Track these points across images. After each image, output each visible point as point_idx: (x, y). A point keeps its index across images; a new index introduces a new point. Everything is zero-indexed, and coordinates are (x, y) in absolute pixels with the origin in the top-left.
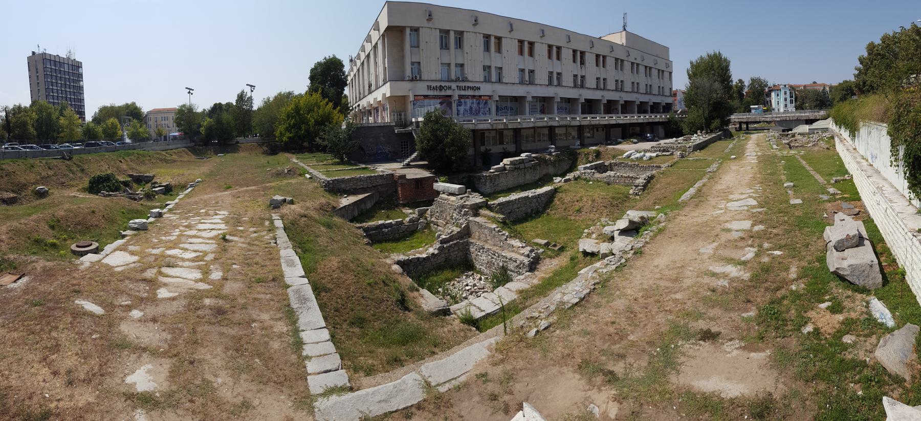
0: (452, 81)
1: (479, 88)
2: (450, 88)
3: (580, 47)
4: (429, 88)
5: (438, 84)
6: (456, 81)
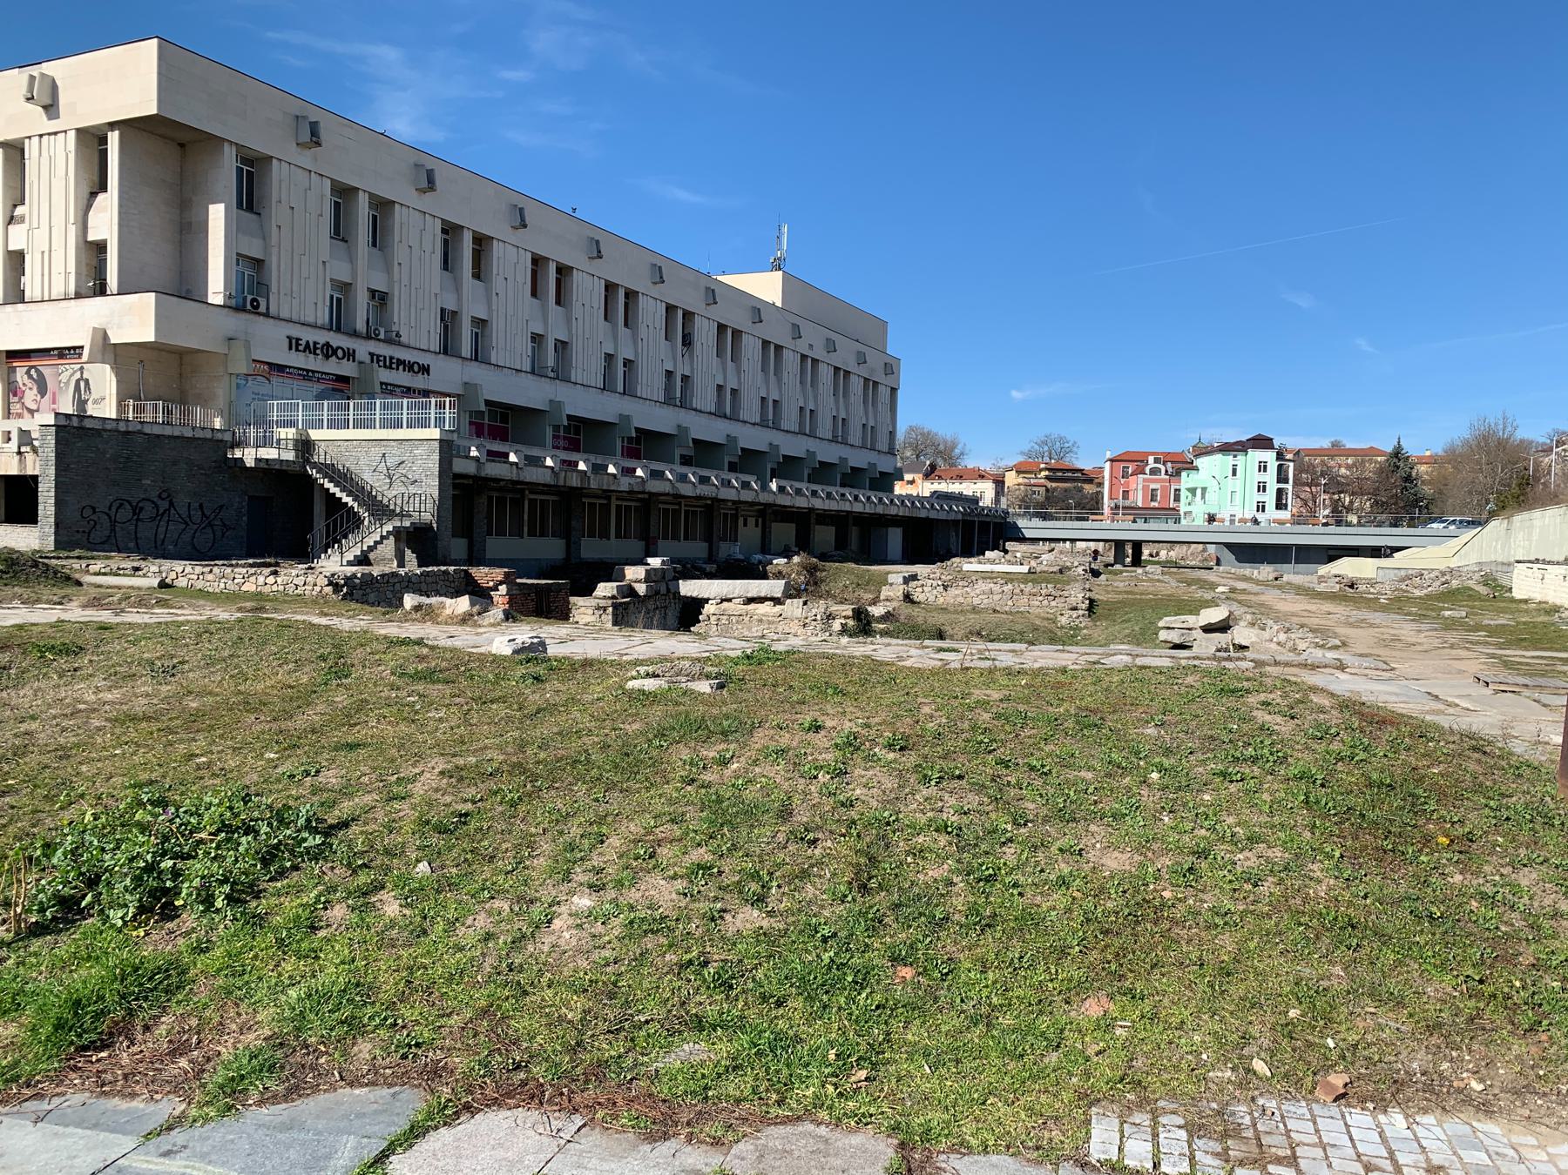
0: (355, 334)
1: (425, 370)
2: (350, 355)
4: (294, 344)
5: (322, 337)
6: (368, 337)
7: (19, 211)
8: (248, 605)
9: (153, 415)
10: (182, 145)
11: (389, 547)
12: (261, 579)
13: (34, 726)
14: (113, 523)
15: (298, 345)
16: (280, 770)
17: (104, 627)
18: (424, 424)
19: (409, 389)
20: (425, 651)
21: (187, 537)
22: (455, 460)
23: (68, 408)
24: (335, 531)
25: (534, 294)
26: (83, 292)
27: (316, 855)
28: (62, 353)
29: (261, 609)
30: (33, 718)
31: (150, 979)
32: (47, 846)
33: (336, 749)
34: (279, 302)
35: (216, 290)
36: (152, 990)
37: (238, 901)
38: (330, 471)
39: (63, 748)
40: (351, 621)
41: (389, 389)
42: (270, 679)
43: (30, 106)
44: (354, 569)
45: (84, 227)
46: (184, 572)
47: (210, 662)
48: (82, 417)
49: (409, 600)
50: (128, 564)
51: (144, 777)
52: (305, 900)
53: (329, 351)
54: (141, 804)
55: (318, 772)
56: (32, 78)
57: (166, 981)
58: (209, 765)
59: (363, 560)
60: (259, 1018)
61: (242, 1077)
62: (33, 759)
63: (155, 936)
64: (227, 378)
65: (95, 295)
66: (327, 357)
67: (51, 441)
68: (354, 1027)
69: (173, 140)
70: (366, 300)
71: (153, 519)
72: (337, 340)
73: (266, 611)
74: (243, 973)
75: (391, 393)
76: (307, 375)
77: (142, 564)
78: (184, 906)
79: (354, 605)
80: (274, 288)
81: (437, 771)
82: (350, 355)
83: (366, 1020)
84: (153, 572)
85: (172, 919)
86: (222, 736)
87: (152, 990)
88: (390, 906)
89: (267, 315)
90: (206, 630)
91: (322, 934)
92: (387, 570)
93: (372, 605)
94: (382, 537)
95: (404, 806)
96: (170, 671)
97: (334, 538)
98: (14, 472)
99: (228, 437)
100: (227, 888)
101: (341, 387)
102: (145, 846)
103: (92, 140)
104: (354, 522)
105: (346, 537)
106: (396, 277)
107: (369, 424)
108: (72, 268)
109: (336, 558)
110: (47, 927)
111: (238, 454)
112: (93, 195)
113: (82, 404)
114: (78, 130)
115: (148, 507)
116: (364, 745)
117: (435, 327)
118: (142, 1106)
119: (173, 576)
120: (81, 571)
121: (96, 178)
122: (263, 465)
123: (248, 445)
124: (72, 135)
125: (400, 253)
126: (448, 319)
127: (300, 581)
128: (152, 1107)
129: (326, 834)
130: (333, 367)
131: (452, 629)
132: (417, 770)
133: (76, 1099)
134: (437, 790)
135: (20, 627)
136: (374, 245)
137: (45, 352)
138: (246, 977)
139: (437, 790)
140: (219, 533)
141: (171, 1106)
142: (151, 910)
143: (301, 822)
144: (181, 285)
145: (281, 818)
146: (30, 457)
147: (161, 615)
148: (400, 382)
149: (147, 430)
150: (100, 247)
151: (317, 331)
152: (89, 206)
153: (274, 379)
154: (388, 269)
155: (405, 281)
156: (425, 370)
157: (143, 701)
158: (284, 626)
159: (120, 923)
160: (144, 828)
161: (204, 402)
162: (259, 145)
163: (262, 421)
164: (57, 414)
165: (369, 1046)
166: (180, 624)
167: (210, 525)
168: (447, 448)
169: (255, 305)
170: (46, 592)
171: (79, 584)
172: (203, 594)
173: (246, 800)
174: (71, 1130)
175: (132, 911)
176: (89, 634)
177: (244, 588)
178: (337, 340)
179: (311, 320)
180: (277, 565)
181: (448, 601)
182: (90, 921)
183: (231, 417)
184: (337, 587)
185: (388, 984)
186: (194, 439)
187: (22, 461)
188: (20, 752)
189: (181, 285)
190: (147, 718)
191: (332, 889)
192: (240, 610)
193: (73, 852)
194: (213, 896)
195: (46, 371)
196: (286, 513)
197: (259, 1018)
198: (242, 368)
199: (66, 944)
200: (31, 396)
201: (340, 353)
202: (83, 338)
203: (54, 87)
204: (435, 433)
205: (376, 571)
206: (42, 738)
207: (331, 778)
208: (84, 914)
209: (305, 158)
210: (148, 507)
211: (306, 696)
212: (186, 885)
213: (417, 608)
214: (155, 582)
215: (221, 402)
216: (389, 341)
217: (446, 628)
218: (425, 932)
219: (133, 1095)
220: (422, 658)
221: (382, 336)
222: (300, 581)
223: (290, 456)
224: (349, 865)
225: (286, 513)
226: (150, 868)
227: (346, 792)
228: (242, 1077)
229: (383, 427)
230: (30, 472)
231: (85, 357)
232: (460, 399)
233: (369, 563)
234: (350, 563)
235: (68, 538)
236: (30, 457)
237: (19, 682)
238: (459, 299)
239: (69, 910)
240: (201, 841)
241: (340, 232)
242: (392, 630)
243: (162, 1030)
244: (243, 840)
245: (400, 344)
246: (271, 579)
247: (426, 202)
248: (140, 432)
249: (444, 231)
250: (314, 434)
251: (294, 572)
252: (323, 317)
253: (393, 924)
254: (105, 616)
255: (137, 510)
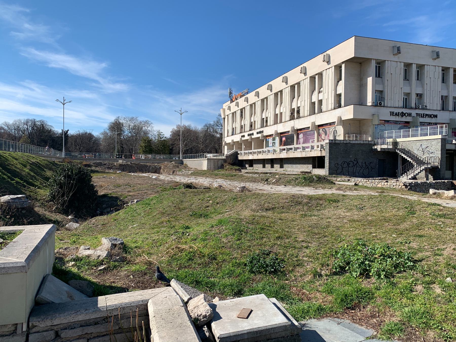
0: (411, 108)
1: (436, 116)
2: (410, 115)
3: (415, 59)
4: (392, 114)
5: (400, 111)
6: (416, 108)
7: (321, 89)
8: (379, 191)
9: (352, 138)
10: (360, 63)
11: (423, 173)
12: (383, 183)
13: (330, 220)
14: (343, 168)
15: (393, 114)
16: (397, 240)
17: (344, 196)
18: (435, 134)
19: (430, 123)
20: (442, 208)
21: (361, 171)
22: (447, 145)
23: (332, 138)
24: (405, 169)
25: (443, 81)
26: (336, 107)
27: (411, 268)
28: (331, 124)
29: (383, 192)
30: (330, 218)
31: (364, 294)
32: (336, 252)
33: (415, 236)
34: (388, 102)
35: (369, 102)
36: (365, 297)
37: (388, 277)
38: (403, 151)
39: (338, 227)
40: (414, 197)
41: (422, 124)
42: (390, 212)
43: (324, 63)
44: (412, 181)
45: (336, 90)
46: (361, 181)
47: (372, 207)
48: (335, 140)
49: (431, 191)
50: (347, 179)
51: (359, 237)
52: (408, 282)
53: (403, 114)
54: (359, 244)
55: (410, 243)
56: (324, 55)
57: (368, 296)
58: (376, 236)
59: (414, 178)
60: (396, 314)
61: (393, 330)
62: (331, 229)
63: (365, 282)
64: (372, 126)
65: (338, 108)
66: (402, 116)
67: (328, 147)
68: (427, 326)
69: (358, 62)
70: (415, 97)
71: (352, 166)
72: (405, 111)
73: (385, 193)
74: (390, 299)
75: (423, 125)
76: (396, 122)
77: (350, 179)
78: (372, 275)
79: (412, 192)
80: (386, 98)
81: (452, 248)
82: (410, 115)
83: (431, 325)
84: (354, 181)
85: (369, 278)
86: (379, 228)
87: (365, 297)
88: (438, 290)
89: (384, 106)
90: (371, 198)
91: (414, 293)
92: (423, 181)
93: (418, 192)
94: (421, 171)
95: (441, 258)
96: (361, 209)
97: (405, 171)
98: (320, 155)
99: (373, 143)
100: (384, 273)
101: (407, 125)
102: (361, 257)
103: (338, 68)
104: (412, 166)
105: (408, 171)
106: (425, 88)
107: (426, 135)
108: (333, 102)
109: (405, 177)
110: (337, 273)
111: (376, 147)
112: (338, 82)
113: (335, 137)
114: (335, 66)
115: (351, 163)
116: (425, 236)
117: (439, 102)
118: (364, 329)
119: (358, 182)
120: (335, 180)
121: (339, 77)
122: (383, 150)
123: (378, 144)
124: (333, 67)
125: (427, 80)
126: (444, 99)
127: (395, 184)
128: (367, 330)
129: (414, 263)
130: (404, 119)
131: (448, 201)
132: (444, 247)
133: (348, 321)
134: (452, 255)
135: (324, 195)
136: (418, 79)
137: (326, 124)
138: (391, 300)
139: (452, 255)
140: (370, 170)
141: (372, 332)
142: (363, 275)
143: (406, 257)
144: (360, 102)
145: (400, 255)
146: (323, 151)
147: (355, 193)
148: (428, 121)
149: (351, 142)
150: (340, 95)
151: (399, 109)
152: (337, 85)
153: (386, 125)
154: (423, 86)
155: (428, 89)
156: (436, 116)
157: (356, 216)
158: (393, 197)
159: (355, 276)
160: (360, 251)
161: (366, 133)
162: (382, 58)
163: (383, 137)
164: (329, 140)
165: (433, 333)
166: (363, 196)
167: (368, 168)
168: (444, 141)
169: (380, 104)
170: (327, 186)
171: (335, 184)
172: (366, 187)
173: (388, 247)
174: (346, 329)
175: (358, 274)
176: (341, 197)
177: (378, 186)
178: (405, 111)
179: (397, 106)
180: (387, 179)
181: (446, 192)
182: (348, 274)
183: (374, 137)
184: (406, 187)
185: (439, 316)
186: (364, 144)
187: (321, 153)
188: (328, 227)
189: (360, 102)
190: (358, 221)
191: (417, 280)
192: (377, 192)
193: (342, 254)
194: (380, 274)
195: (327, 129)
196: (390, 164)
197: (396, 314)
198: (377, 122)
199: (342, 279)
200: (323, 136)
201: (406, 115)
202: (335, 120)
203: (329, 56)
204: (440, 136)
205: (419, 181)
206: (332, 223)
207: (414, 245)
208: (346, 272)
209: (396, 58)
210: (351, 163)
211: (403, 219)
212: (373, 269)
213: (435, 194)
214: (354, 184)
215: (371, 133)
216: (423, 109)
217: (445, 201)
218: (451, 301)
219: (362, 325)
220: (441, 210)
221: (420, 108)
222: (395, 184)
223: (391, 147)
224: (422, 274)
225: (390, 164)
226: (363, 263)
227: (420, 250)
228: (393, 330)
229: (421, 136)
230: (323, 155)
231: (336, 125)
232: (449, 124)
233: (416, 179)
234: (410, 179)
235: (334, 171)
236: (323, 151)
237: (325, 208)
238: (448, 92)
239: (342, 270)
240: (376, 258)
241: (406, 78)
242: (425, 200)
243: (368, 309)
244: (388, 259)
245: (426, 109)
246: (386, 183)
247: (437, 62)
248: (349, 143)
249: (443, 70)
250: (398, 140)
251: (393, 182)
252: (401, 104)
253: (439, 296)
254: (341, 192)
255: (348, 164)
